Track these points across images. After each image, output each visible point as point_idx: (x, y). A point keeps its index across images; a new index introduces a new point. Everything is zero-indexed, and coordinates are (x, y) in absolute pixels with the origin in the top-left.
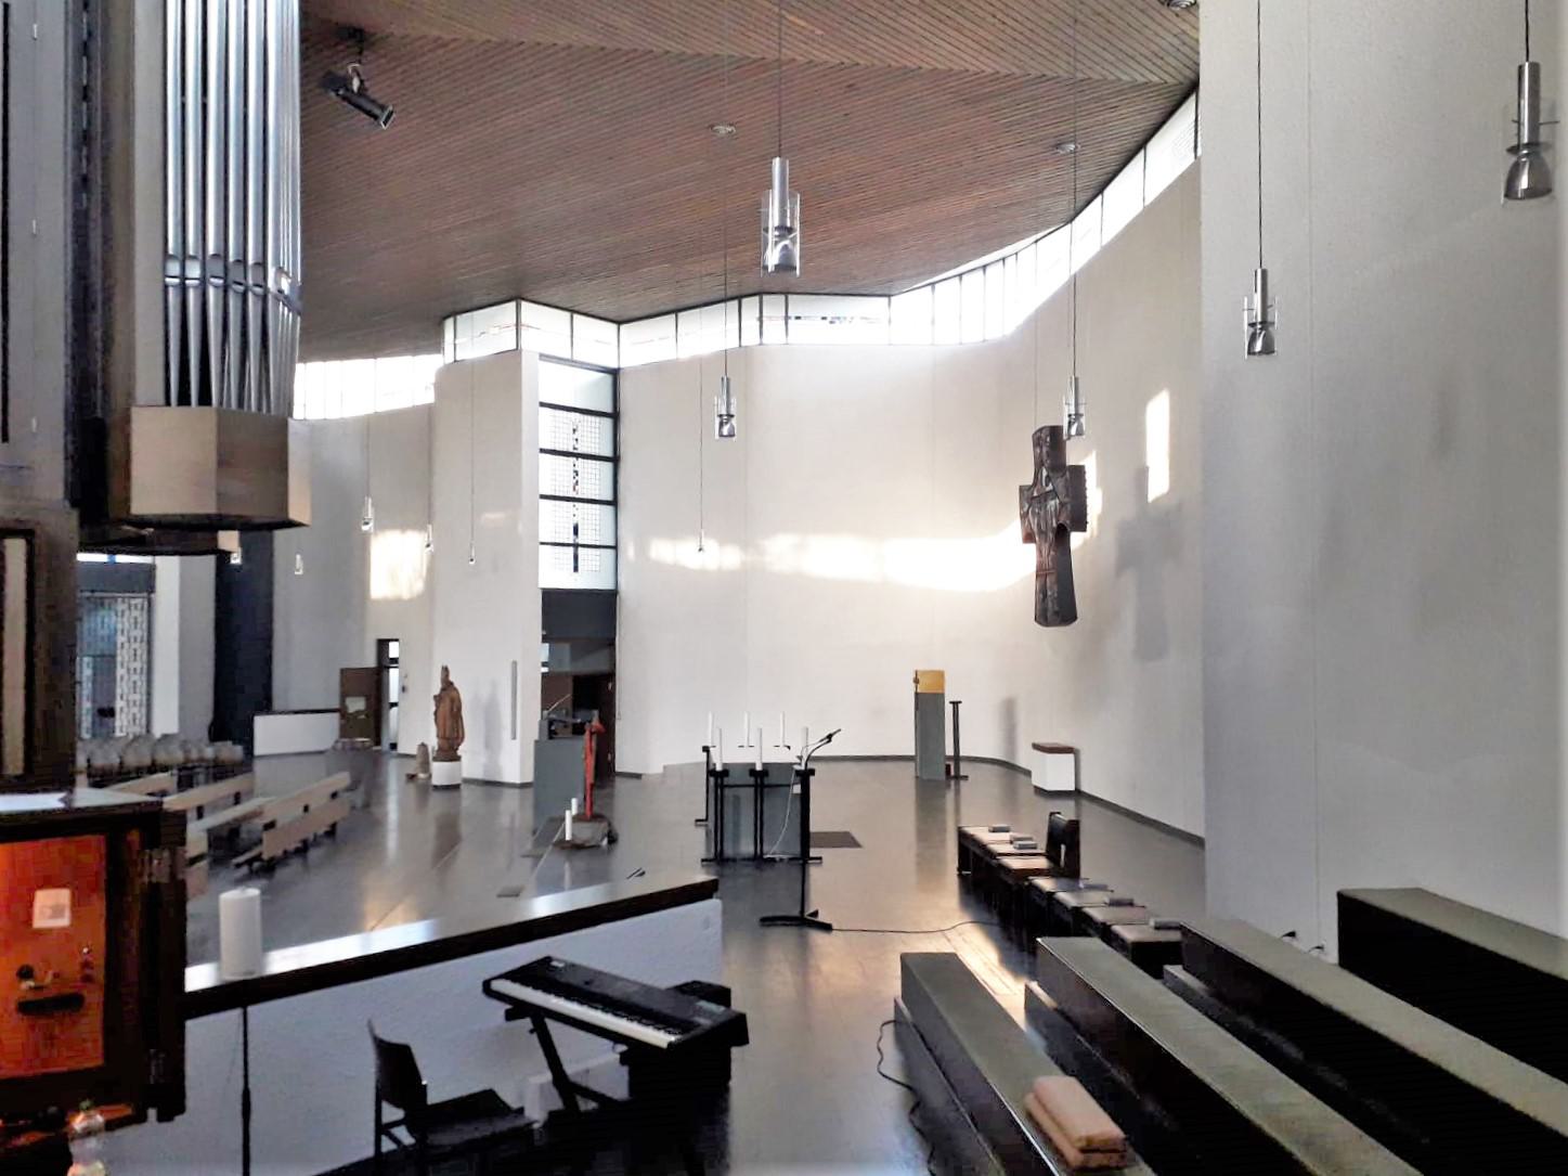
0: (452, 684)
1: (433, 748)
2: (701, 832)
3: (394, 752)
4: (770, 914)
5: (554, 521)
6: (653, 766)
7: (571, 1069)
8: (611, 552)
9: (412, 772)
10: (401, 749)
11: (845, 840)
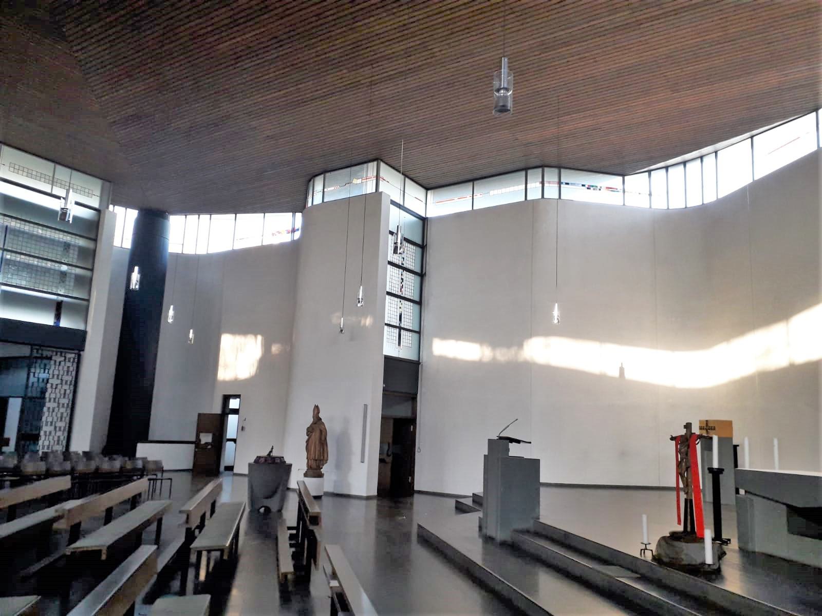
0: (321, 419)
10: (236, 471)
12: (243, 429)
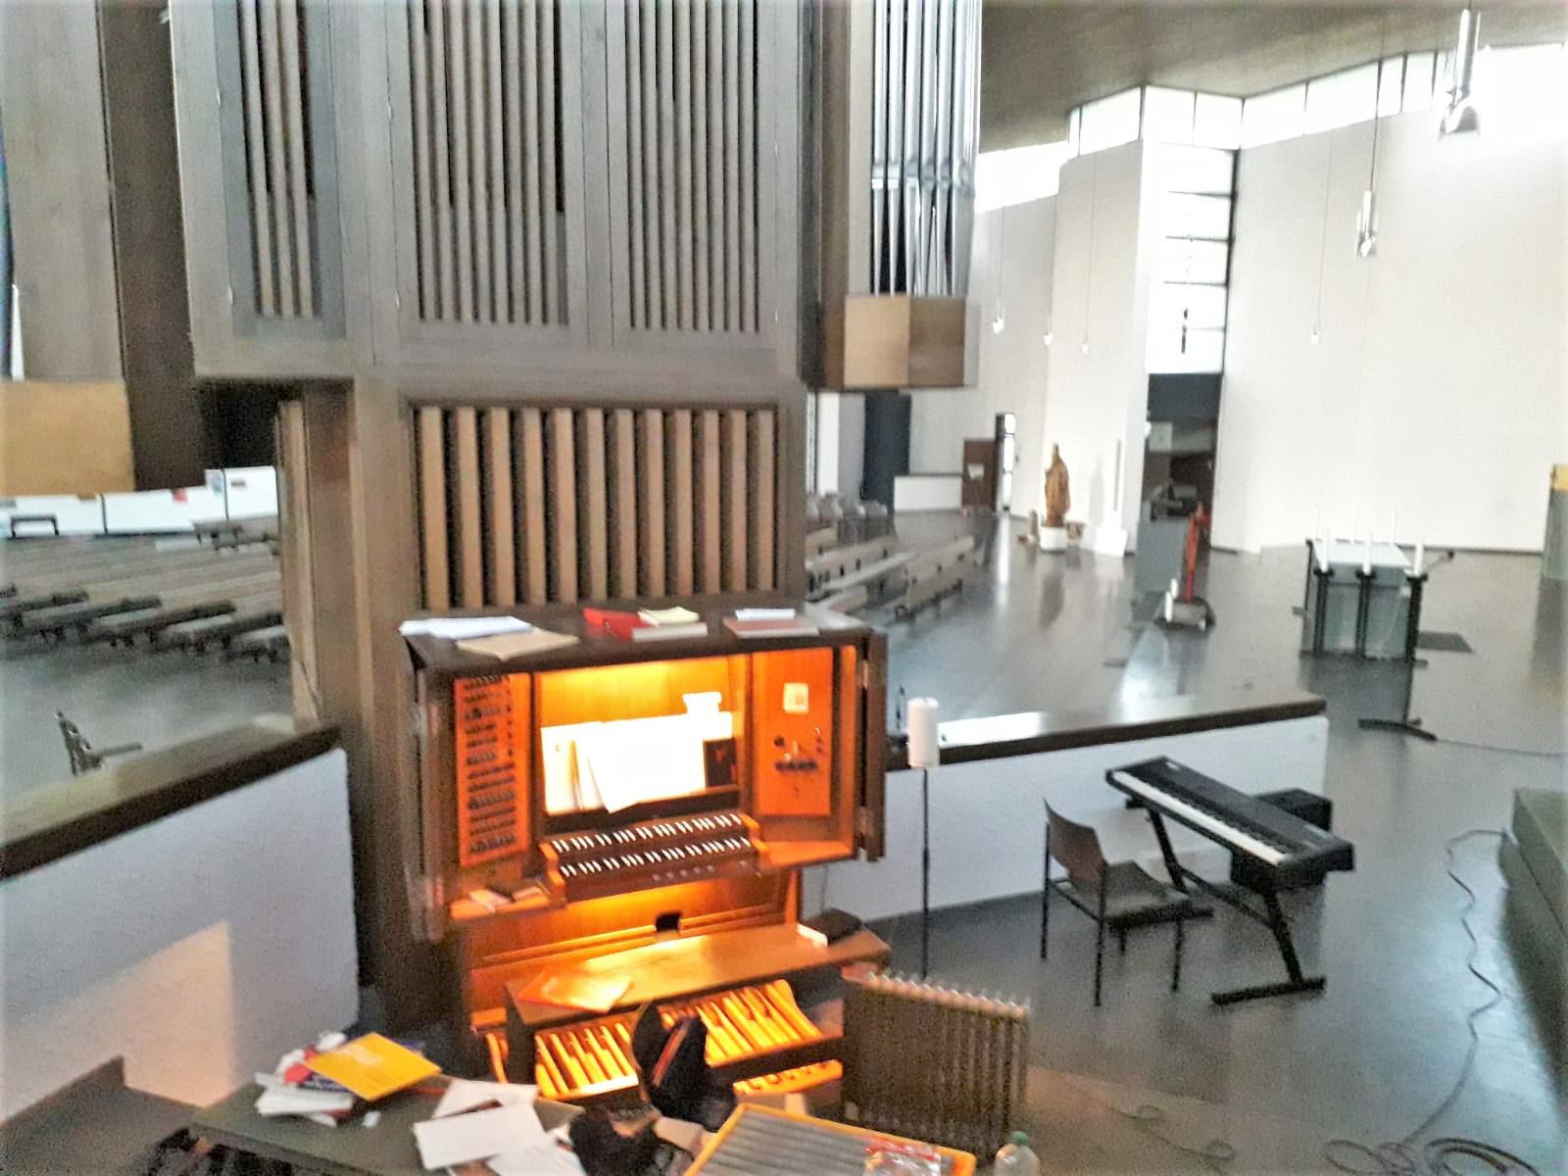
1: (1043, 517)
2: (1299, 622)
4: (1371, 717)
6: (1252, 545)
9: (1022, 533)
10: (1013, 511)
11: (1454, 643)
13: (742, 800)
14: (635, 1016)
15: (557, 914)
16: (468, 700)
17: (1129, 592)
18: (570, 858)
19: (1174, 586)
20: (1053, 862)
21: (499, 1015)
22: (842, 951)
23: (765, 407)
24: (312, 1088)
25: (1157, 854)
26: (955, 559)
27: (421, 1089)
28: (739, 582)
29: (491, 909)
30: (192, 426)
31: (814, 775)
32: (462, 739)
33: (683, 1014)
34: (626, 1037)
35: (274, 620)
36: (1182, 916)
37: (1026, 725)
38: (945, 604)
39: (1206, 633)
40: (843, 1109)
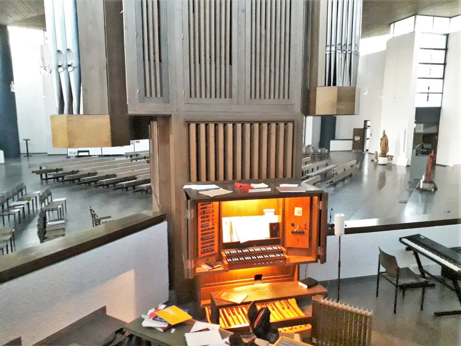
0: (386, 135)
3: (367, 152)
5: (422, 86)
7: (423, 264)
8: (441, 94)
9: (373, 159)
10: (369, 152)
12: (371, 135)
13: (281, 242)
14: (249, 306)
15: (226, 273)
16: (202, 209)
17: (408, 178)
18: (229, 256)
19: (424, 177)
20: (381, 266)
21: (209, 302)
22: (311, 291)
23: (290, 122)
24: (157, 320)
25: (416, 265)
26: (350, 167)
27: (187, 323)
28: (281, 176)
29: (207, 270)
30: (126, 129)
31: (304, 236)
32: (200, 220)
33: (263, 306)
34: (246, 312)
35: (148, 181)
36: (425, 286)
37: (373, 222)
38: (346, 181)
39: (434, 192)
40: (311, 340)
